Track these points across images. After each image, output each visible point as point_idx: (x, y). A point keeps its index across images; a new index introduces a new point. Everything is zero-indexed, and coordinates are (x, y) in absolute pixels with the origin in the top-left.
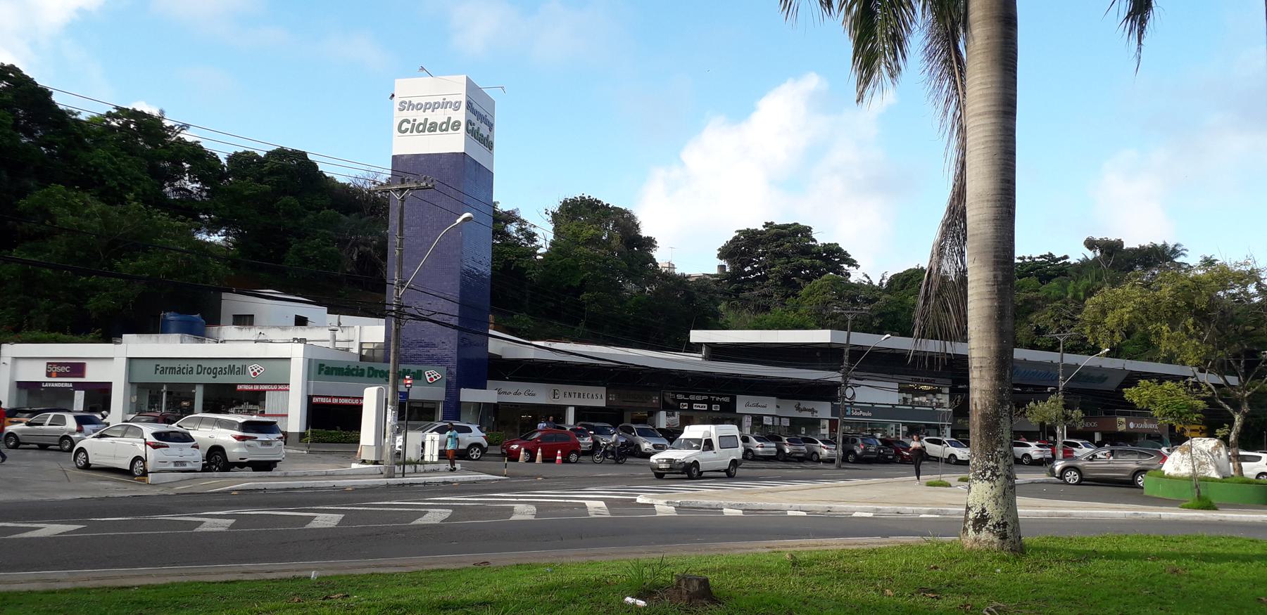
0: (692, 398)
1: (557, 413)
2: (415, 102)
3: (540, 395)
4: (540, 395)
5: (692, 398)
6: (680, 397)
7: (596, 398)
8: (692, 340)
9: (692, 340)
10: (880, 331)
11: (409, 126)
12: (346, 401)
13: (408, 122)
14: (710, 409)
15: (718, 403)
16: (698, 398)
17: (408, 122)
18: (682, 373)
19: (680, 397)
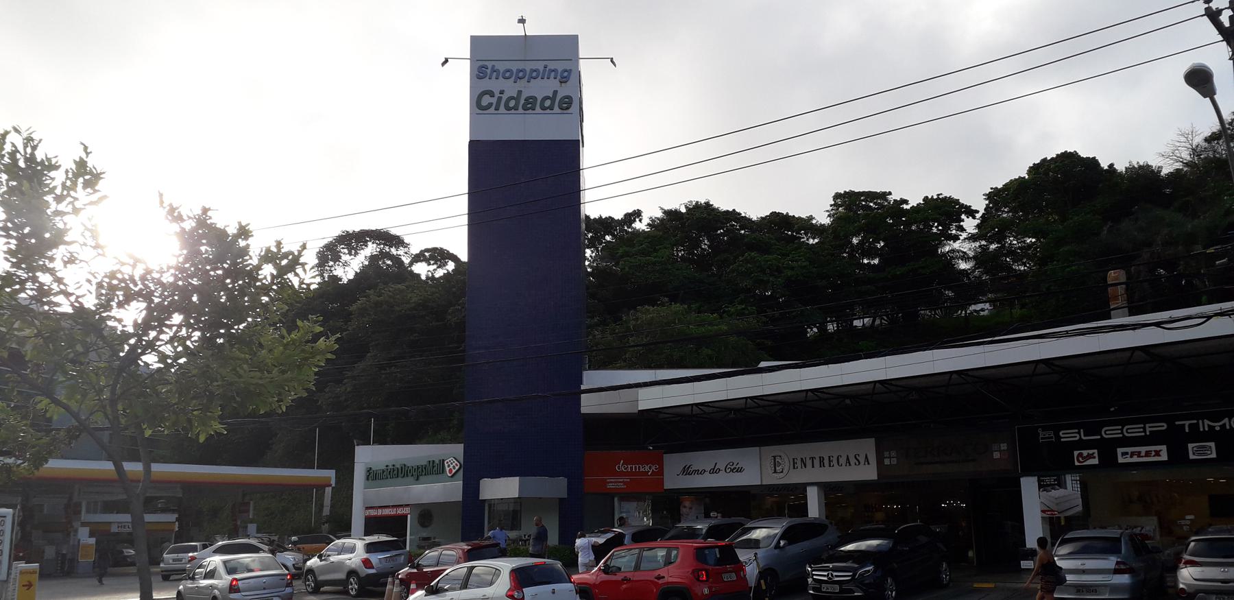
0: (1110, 433)
1: (784, 501)
2: (502, 67)
3: (747, 469)
4: (747, 469)
5: (1110, 433)
6: (1068, 436)
7: (857, 463)
8: (584, 410)
9: (584, 410)
10: (1088, 307)
11: (494, 100)
12: (387, 512)
13: (492, 94)
14: (1178, 456)
15: (1209, 435)
16: (1134, 431)
17: (492, 94)
18: (276, 467)
19: (1068, 436)
